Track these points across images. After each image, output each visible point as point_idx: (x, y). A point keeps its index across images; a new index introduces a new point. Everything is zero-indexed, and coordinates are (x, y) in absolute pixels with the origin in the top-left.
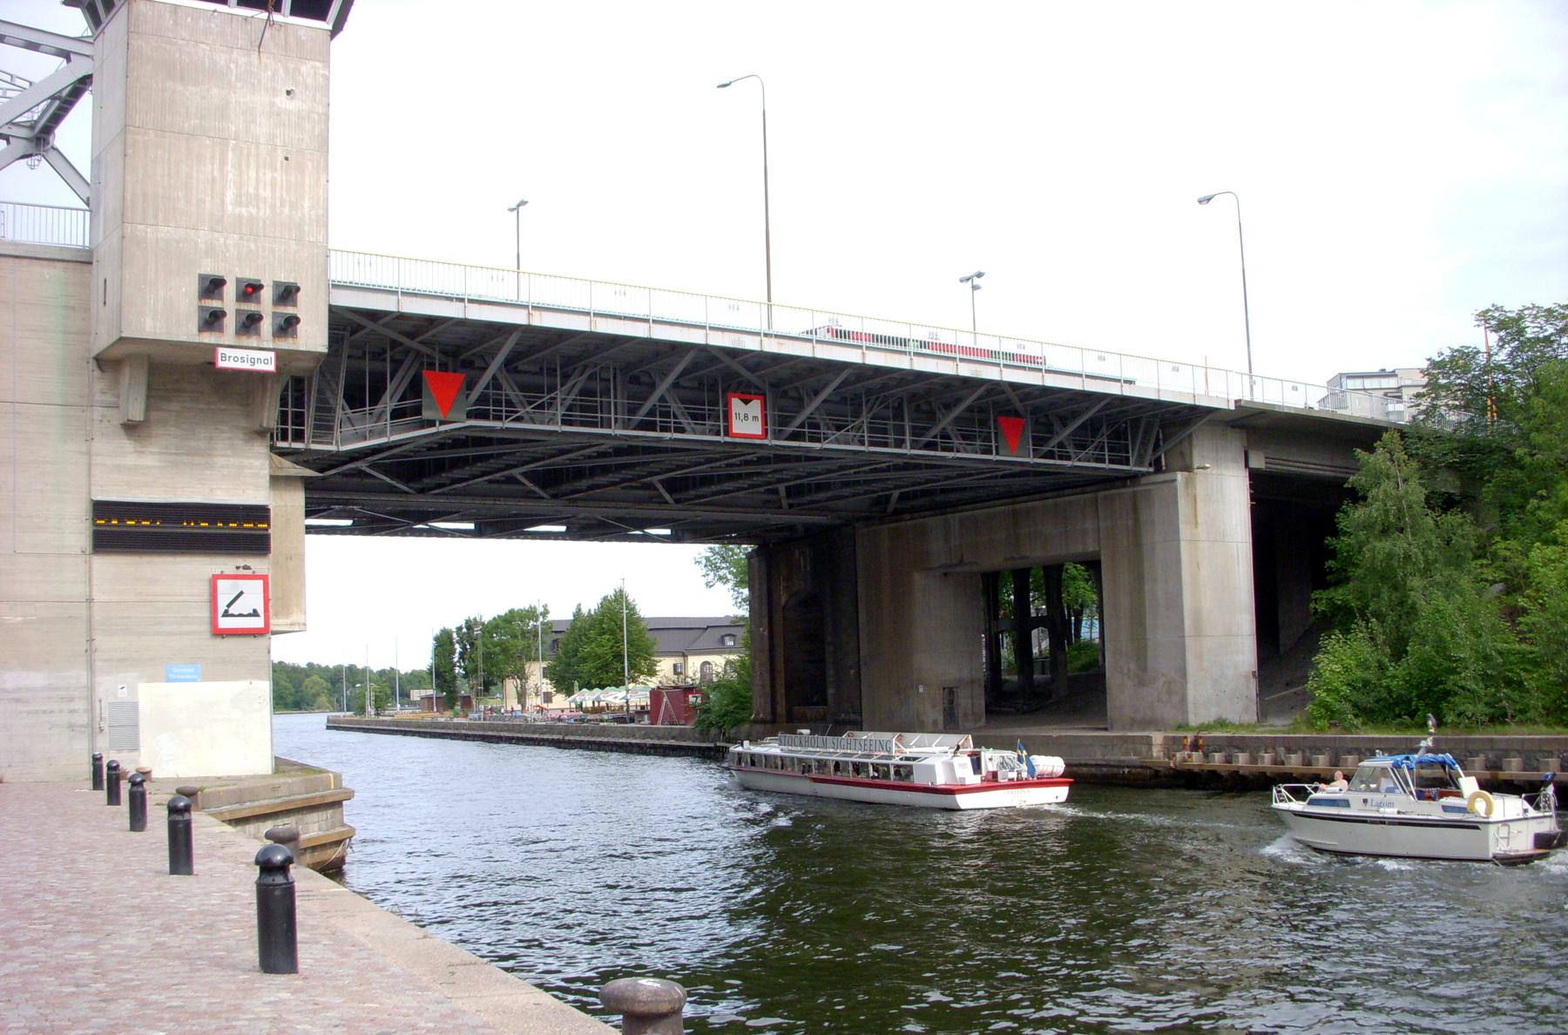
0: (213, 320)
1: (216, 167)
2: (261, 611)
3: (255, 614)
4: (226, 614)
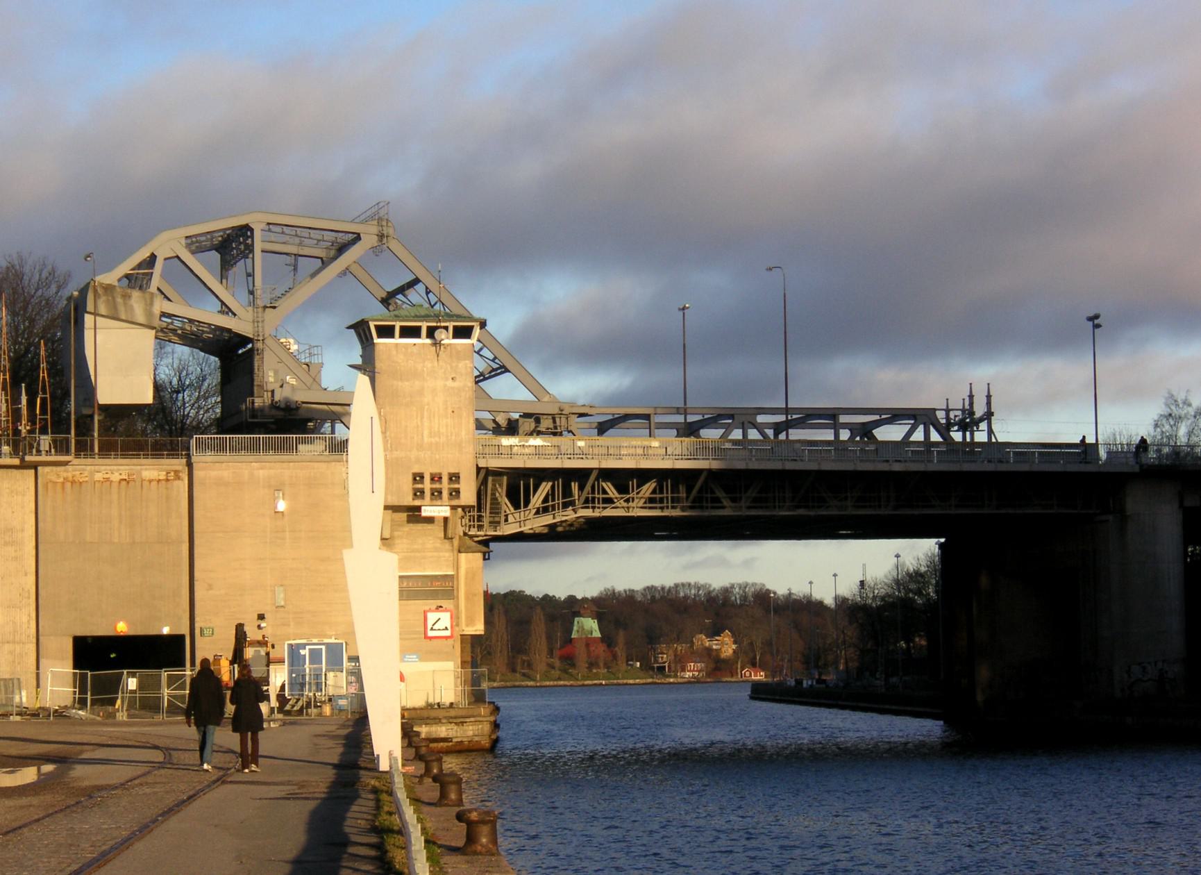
0: (419, 493)
1: (419, 419)
2: (449, 627)
3: (446, 629)
4: (432, 629)
